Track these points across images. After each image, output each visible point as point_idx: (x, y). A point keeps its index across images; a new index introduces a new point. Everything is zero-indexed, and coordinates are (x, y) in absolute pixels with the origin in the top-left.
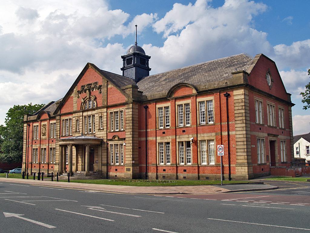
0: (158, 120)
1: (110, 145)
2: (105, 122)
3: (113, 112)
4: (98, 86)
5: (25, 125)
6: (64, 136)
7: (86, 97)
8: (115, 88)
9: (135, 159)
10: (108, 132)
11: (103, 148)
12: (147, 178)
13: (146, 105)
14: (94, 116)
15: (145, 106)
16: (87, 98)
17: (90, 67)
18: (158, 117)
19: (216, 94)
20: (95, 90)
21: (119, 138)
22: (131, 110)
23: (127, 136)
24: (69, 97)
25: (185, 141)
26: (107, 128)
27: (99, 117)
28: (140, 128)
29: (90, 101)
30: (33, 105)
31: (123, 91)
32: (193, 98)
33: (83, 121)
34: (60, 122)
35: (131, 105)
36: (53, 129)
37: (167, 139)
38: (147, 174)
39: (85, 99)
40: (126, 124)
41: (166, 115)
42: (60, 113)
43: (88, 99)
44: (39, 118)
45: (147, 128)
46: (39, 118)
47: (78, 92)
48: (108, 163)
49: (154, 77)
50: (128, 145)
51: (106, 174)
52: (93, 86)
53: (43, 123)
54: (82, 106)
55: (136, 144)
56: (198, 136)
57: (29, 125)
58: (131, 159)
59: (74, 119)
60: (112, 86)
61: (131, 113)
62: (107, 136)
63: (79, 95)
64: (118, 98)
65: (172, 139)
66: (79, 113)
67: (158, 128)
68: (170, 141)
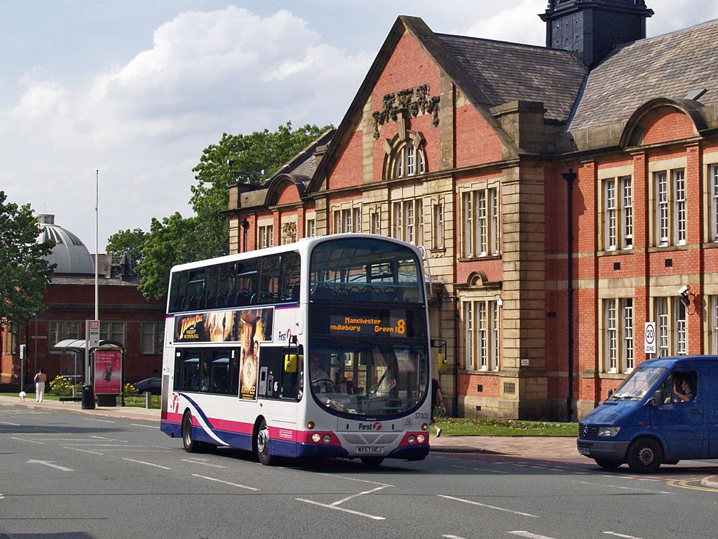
0: (603, 222)
1: (464, 302)
2: (449, 225)
3: (472, 193)
4: (428, 99)
5: (234, 223)
6: (471, 260)
7: (397, 136)
8: (474, 112)
9: (533, 354)
10: (458, 261)
11: (444, 315)
12: (573, 416)
13: (571, 170)
14: (419, 202)
15: (566, 171)
16: (399, 140)
17: (407, 32)
18: (603, 213)
19: (638, 159)
20: (420, 113)
21: (485, 279)
22: (517, 188)
23: (506, 276)
24: (353, 134)
25: (672, 298)
26: (455, 247)
27: (433, 206)
28: (552, 247)
29: (409, 149)
30: (294, 129)
31: (496, 121)
32: (691, 151)
33: (390, 219)
34: (328, 219)
35: (517, 170)
36: (672, 201)
37: (624, 286)
38: (573, 403)
39: (396, 143)
40: (506, 236)
41: (610, 207)
42: (328, 188)
43: (405, 143)
44: (273, 198)
45: (574, 249)
46: (273, 198)
47: (374, 115)
48: (457, 364)
49: (674, 40)
50: (509, 304)
51: (451, 402)
52: (415, 99)
53: (286, 219)
54: (388, 166)
55: (534, 304)
56: (705, 282)
57: (246, 225)
58: (517, 353)
59: (366, 209)
60: (468, 103)
61: (516, 198)
62: (455, 275)
63: (380, 127)
64: (484, 147)
65: (636, 288)
66: (378, 192)
67: (603, 250)
68: (631, 293)
